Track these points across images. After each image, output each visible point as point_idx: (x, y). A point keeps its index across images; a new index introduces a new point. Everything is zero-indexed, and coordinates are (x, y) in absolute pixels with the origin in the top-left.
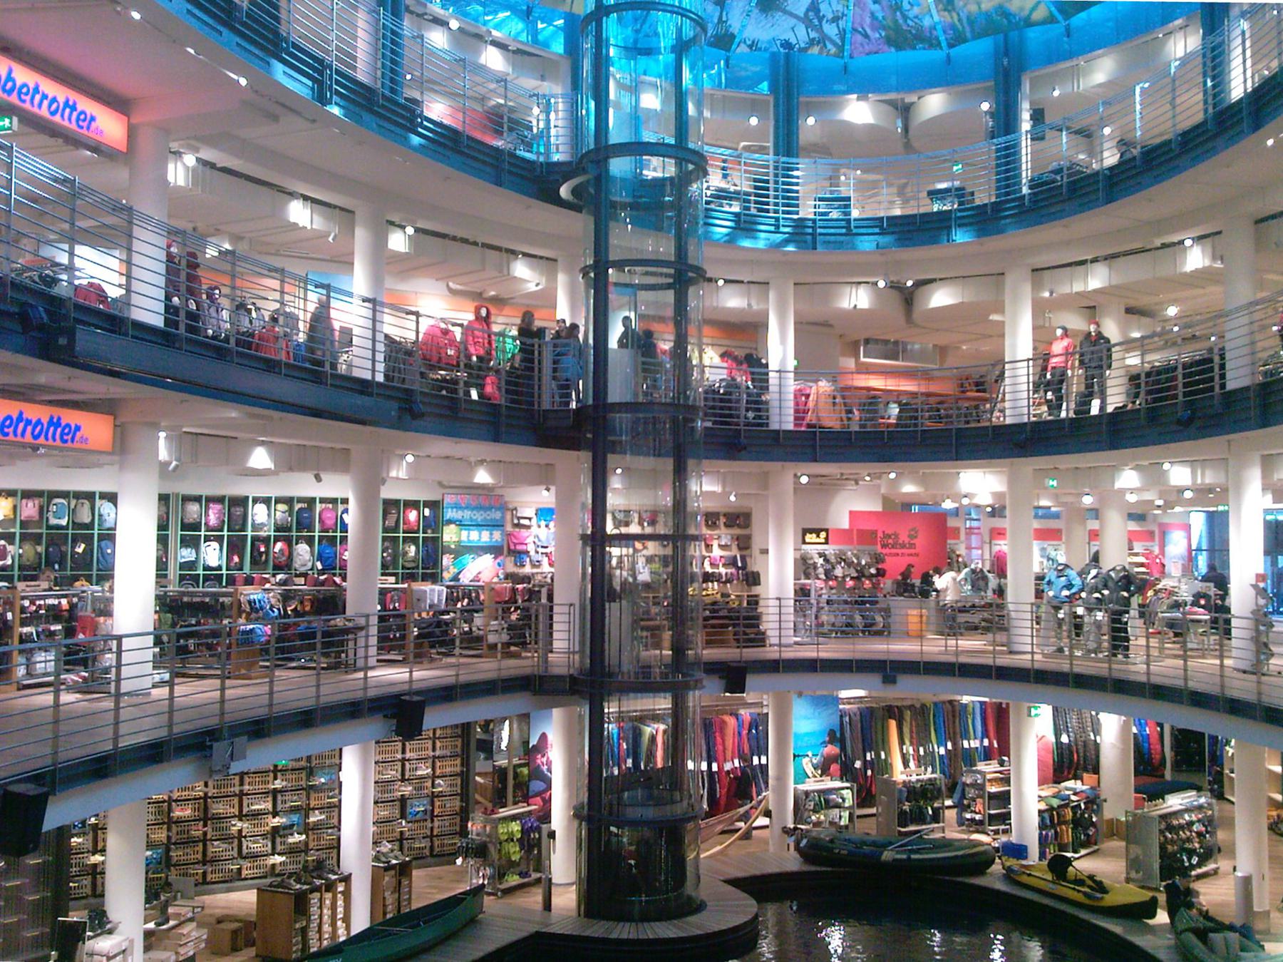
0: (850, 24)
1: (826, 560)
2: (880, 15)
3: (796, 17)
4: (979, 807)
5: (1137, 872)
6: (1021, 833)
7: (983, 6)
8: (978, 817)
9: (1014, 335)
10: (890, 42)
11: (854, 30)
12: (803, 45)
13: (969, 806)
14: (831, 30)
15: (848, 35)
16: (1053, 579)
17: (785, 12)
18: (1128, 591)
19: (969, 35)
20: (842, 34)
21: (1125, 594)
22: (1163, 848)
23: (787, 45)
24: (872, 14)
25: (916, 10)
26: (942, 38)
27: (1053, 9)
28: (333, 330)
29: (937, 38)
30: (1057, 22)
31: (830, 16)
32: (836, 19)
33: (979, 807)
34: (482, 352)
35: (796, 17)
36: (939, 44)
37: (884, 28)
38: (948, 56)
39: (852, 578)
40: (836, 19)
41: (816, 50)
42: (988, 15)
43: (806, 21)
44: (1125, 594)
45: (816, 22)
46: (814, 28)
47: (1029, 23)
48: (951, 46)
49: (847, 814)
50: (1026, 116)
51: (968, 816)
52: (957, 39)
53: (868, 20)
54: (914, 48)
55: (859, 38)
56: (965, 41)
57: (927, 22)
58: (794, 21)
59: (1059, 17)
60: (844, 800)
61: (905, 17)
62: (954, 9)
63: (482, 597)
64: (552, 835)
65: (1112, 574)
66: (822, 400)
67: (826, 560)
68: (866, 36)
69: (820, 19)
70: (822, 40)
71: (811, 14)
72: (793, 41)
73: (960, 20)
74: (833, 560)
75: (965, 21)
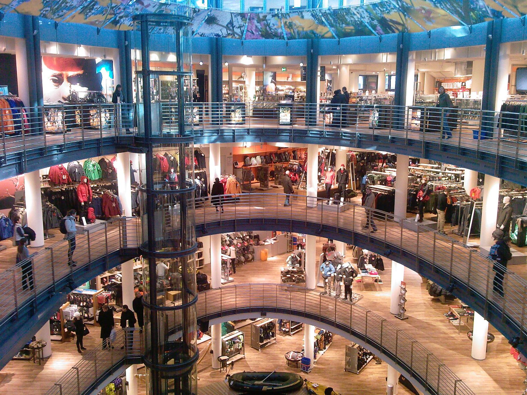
0: (246, 29)
1: (230, 238)
2: (260, 27)
3: (223, 26)
4: (288, 326)
5: (349, 366)
6: (308, 354)
7: (305, 29)
8: (287, 330)
9: (311, 167)
10: (262, 36)
11: (248, 31)
12: (224, 35)
13: (284, 325)
14: (237, 31)
15: (245, 32)
16: (324, 267)
17: (218, 24)
18: (352, 276)
19: (297, 37)
20: (242, 32)
21: (351, 277)
22: (359, 358)
23: (218, 35)
24: (256, 27)
25: (275, 27)
26: (285, 36)
27: (334, 34)
28: (21, 240)
29: (283, 36)
30: (335, 38)
31: (238, 26)
32: (240, 27)
33: (288, 326)
34: (86, 200)
35: (223, 26)
36: (284, 38)
37: (261, 31)
38: (287, 43)
39: (240, 243)
40: (240, 27)
41: (230, 37)
42: (306, 32)
43: (227, 27)
44: (351, 277)
45: (231, 28)
46: (230, 30)
47: (323, 37)
48: (288, 39)
49: (241, 344)
50: (319, 69)
51: (284, 329)
52: (291, 37)
53: (254, 28)
54: (273, 38)
55: (249, 34)
56: (295, 39)
57: (280, 31)
58: (221, 27)
59: (336, 37)
60: (240, 340)
61: (271, 29)
62: (292, 28)
63: (92, 301)
64: (127, 384)
65: (347, 269)
66: (232, 186)
67: (230, 238)
68: (253, 33)
69: (233, 27)
70: (234, 34)
71: (229, 25)
72: (220, 34)
73: (294, 32)
74: (233, 237)
75: (296, 33)
